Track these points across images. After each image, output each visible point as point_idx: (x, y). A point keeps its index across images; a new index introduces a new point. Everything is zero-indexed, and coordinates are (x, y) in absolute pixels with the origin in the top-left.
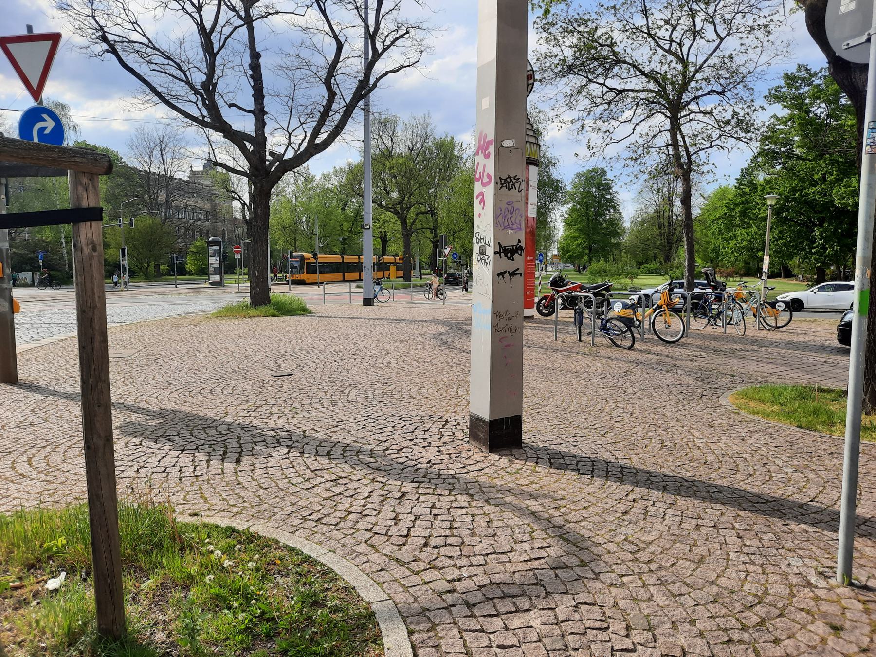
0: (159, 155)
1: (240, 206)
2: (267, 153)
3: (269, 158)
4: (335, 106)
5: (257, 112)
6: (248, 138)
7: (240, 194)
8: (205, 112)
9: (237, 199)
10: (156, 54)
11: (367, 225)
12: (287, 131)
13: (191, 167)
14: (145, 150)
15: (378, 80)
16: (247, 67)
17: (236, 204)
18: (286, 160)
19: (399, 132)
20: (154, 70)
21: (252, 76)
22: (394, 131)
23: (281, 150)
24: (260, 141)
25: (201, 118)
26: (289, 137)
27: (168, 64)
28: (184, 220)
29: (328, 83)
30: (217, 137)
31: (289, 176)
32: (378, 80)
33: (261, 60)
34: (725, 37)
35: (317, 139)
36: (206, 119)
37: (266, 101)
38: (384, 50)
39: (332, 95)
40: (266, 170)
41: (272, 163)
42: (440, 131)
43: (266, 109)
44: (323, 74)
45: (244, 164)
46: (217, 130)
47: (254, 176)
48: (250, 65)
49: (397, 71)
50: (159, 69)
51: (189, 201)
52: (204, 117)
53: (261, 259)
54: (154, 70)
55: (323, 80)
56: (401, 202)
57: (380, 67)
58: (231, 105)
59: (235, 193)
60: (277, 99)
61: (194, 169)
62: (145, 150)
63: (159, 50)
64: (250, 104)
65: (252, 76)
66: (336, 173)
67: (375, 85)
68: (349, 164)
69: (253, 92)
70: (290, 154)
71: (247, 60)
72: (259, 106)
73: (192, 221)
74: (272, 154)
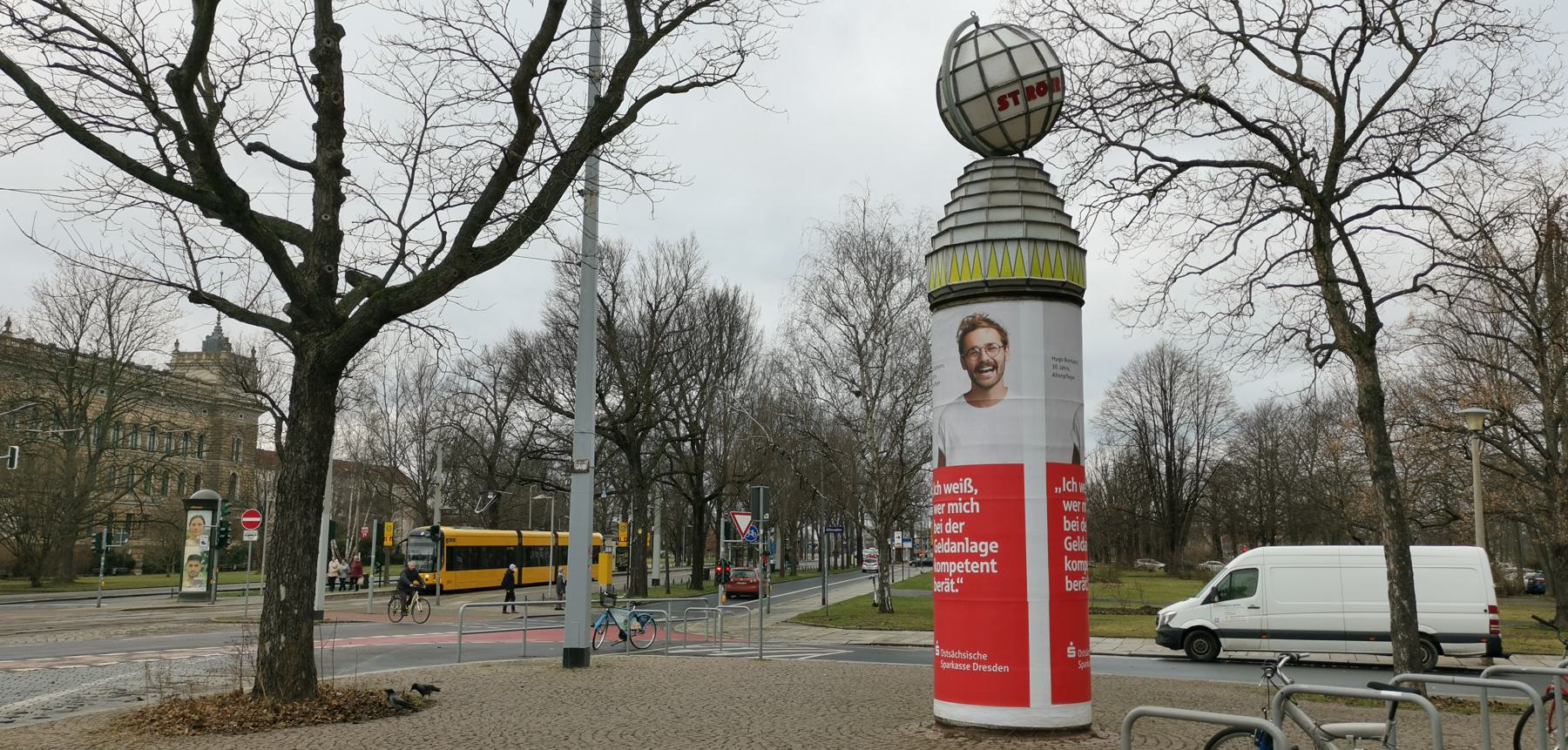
0: (102, 316)
1: (272, 421)
2: (342, 276)
3: (343, 287)
4: (534, 151)
5: (322, 168)
6: (293, 233)
7: (274, 397)
8: (174, 157)
9: (269, 409)
10: (66, 29)
11: (582, 461)
12: (399, 225)
13: (177, 344)
14: (73, 305)
15: (640, 103)
16: (305, 60)
17: (266, 420)
18: (395, 288)
19: (628, 273)
20: (57, 65)
21: (315, 80)
22: (619, 270)
23: (380, 272)
24: (326, 238)
25: (163, 171)
26: (403, 241)
27: (96, 49)
28: (141, 454)
29: (521, 91)
30: (213, 233)
31: (390, 335)
32: (640, 103)
33: (344, 44)
34: (1425, 49)
35: (482, 234)
36: (178, 177)
37: (348, 147)
38: (660, 33)
39: (528, 121)
40: (334, 316)
41: (350, 300)
42: (714, 279)
43: (346, 164)
44: (508, 61)
45: (276, 300)
46: (209, 210)
47: (299, 329)
48: (313, 54)
49: (685, 89)
50: (69, 61)
51: (148, 414)
52: (172, 169)
53: (299, 552)
54: (57, 65)
55: (521, 54)
56: (629, 418)
57: (657, 64)
58: (251, 148)
59: (265, 395)
60: (379, 149)
61: (182, 349)
62: (73, 305)
63: (75, 17)
64: (306, 150)
65: (315, 80)
66: (488, 361)
67: (631, 116)
68: (519, 339)
69: (314, 117)
70: (401, 278)
71: (307, 41)
72: (329, 155)
73: (158, 456)
74: (353, 276)
